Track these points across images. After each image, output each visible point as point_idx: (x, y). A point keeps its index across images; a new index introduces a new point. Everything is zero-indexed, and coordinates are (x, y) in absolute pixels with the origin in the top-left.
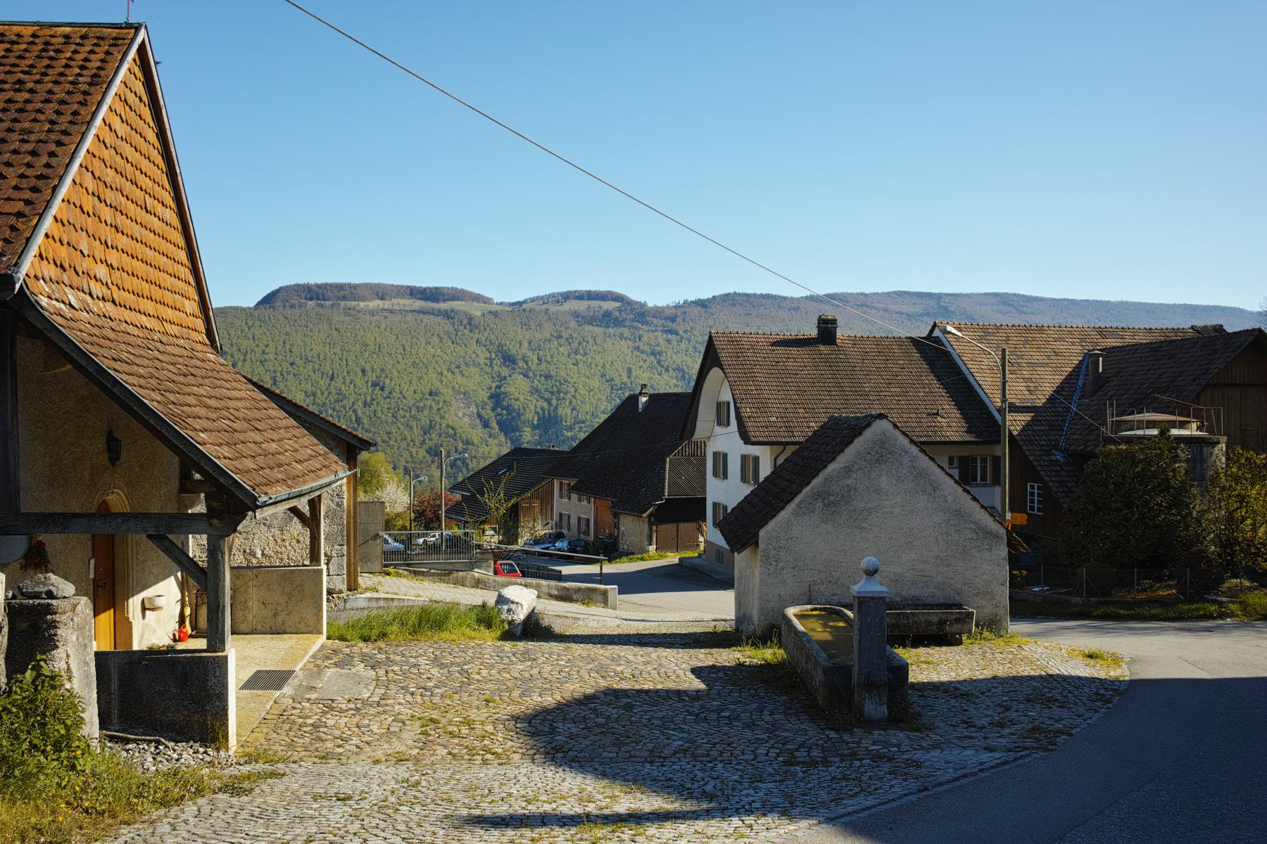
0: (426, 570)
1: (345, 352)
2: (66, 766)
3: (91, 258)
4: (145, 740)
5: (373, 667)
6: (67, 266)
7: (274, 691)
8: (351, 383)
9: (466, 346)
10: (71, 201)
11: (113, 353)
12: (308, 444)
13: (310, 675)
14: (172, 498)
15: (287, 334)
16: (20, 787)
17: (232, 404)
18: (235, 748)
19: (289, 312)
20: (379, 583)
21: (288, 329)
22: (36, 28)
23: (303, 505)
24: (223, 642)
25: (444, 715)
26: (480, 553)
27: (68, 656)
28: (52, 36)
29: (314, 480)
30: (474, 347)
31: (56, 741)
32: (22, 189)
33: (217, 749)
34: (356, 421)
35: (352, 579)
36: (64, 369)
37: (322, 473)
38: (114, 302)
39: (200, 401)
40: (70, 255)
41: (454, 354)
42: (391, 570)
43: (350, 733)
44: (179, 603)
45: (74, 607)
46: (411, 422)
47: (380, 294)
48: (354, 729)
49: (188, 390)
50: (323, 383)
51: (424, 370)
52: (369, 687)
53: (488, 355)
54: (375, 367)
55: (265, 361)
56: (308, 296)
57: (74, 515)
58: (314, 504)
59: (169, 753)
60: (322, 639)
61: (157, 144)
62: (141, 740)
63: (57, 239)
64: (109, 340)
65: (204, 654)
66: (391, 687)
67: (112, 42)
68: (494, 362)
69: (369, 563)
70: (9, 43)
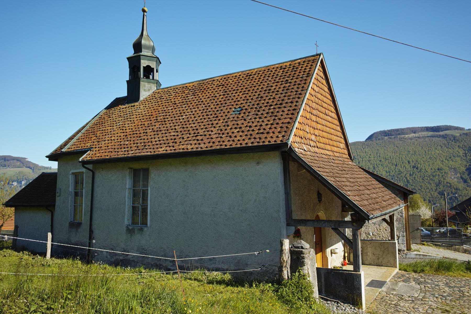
0: (441, 244)
1: (401, 155)
2: (309, 307)
3: (310, 133)
4: (334, 301)
5: (419, 284)
6: (303, 137)
7: (379, 289)
8: (404, 167)
9: (453, 149)
10: (303, 116)
11: (318, 165)
12: (388, 194)
13: (393, 284)
14: (339, 214)
15: (378, 150)
16: (295, 312)
17: (358, 180)
18: (365, 309)
19: (378, 142)
20: (420, 248)
21: (378, 148)
22: (290, 62)
23: (387, 217)
24: (359, 269)
25: (452, 309)
26: (466, 238)
27: (308, 269)
28: (295, 64)
29: (391, 208)
30: (457, 149)
31: (305, 298)
32: (289, 114)
33: (358, 308)
34: (407, 182)
35: (409, 246)
36: (303, 171)
37: (394, 205)
38: (317, 147)
39: (347, 180)
40: (303, 133)
41: (448, 152)
42: (425, 243)
43: (410, 310)
44: (343, 252)
45: (309, 252)
46: (430, 182)
47: (413, 131)
48: (412, 309)
49: (343, 176)
50: (393, 167)
51: (435, 160)
52: (417, 292)
53: (464, 152)
54: (413, 160)
55: (370, 160)
56: (385, 135)
57: (308, 220)
58: (391, 217)
59: (342, 307)
60: (397, 270)
61: (328, 92)
62: (332, 301)
63: (300, 129)
64: (317, 160)
65: (352, 272)
66: (427, 293)
67: (312, 61)
68: (467, 155)
69: (415, 240)
70: (283, 69)
